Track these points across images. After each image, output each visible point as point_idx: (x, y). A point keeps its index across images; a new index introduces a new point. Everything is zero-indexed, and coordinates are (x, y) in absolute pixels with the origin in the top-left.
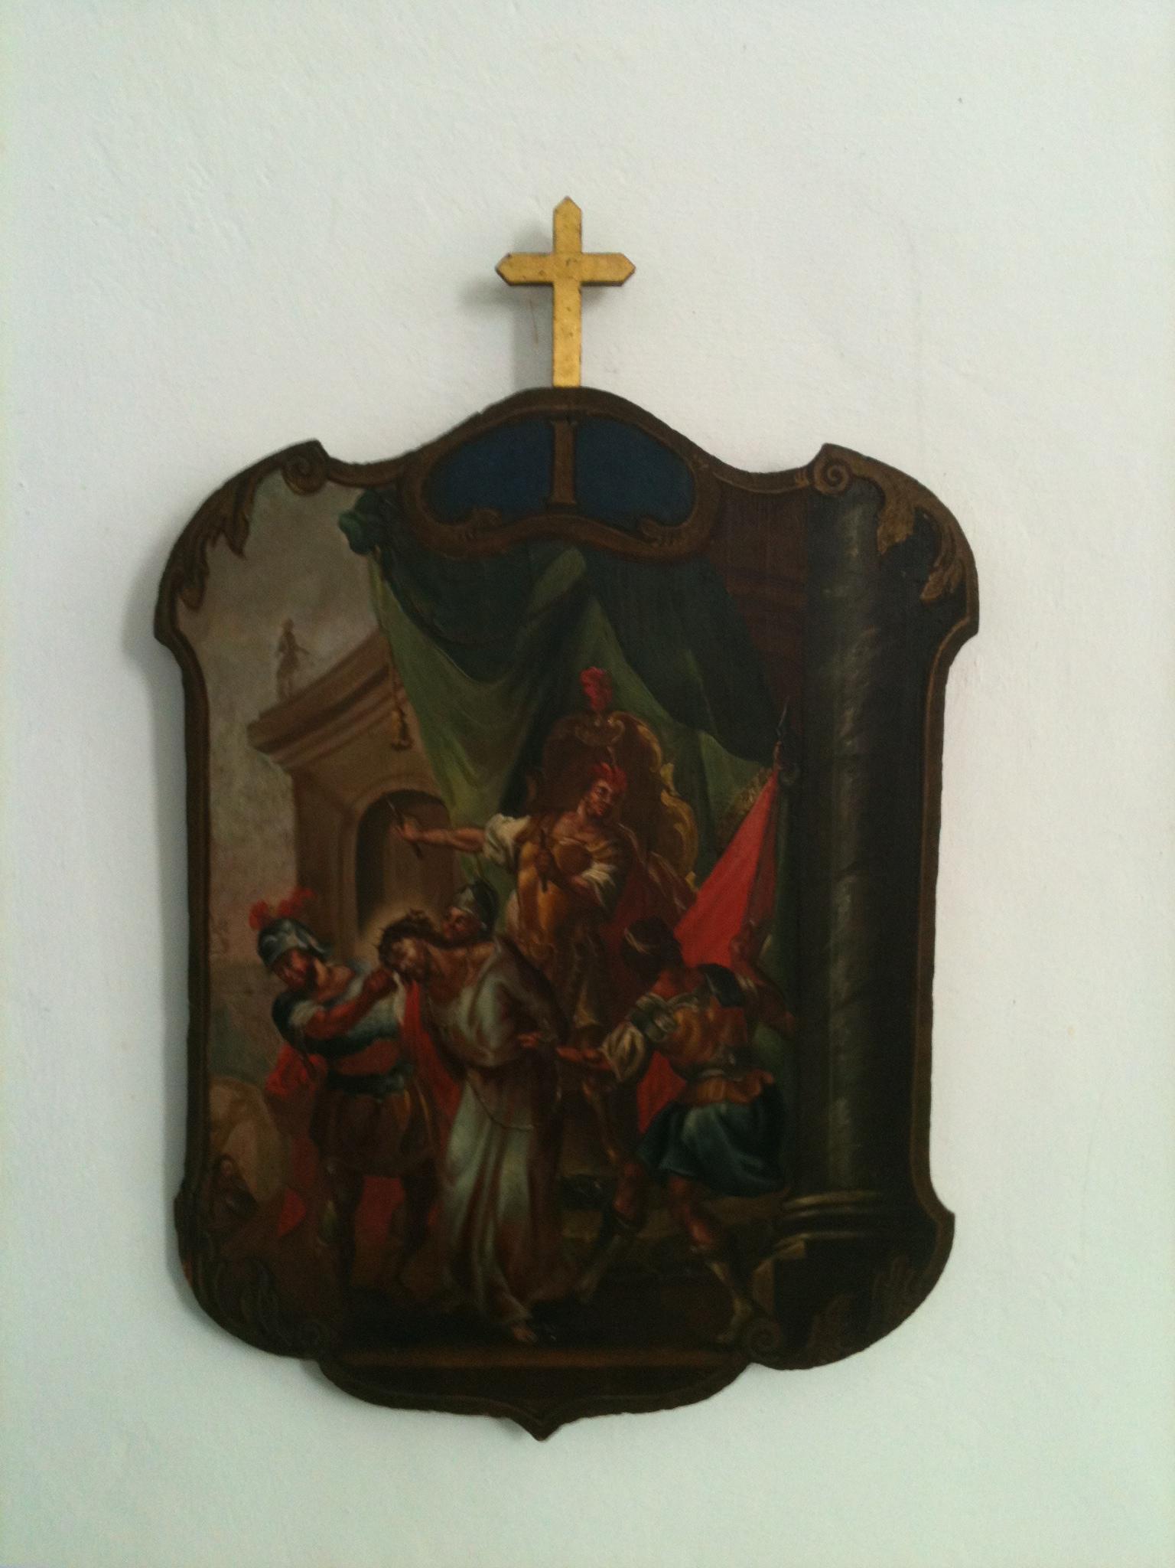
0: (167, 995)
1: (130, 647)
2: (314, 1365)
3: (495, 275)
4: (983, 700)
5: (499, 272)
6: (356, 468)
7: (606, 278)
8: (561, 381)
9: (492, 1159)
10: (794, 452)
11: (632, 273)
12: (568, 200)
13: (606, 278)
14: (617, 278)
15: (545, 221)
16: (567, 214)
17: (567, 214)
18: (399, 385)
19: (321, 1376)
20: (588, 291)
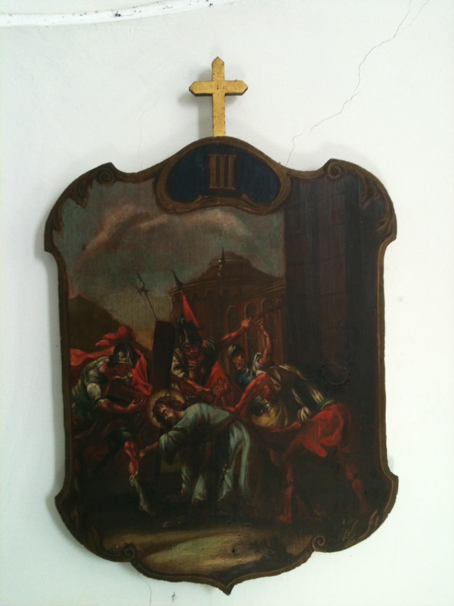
0: (55, 399)
1: (37, 254)
2: (129, 564)
3: (189, 91)
4: (398, 264)
5: (190, 90)
6: (133, 175)
7: (236, 91)
8: (218, 134)
9: (190, 577)
10: (316, 163)
11: (247, 89)
12: (217, 58)
13: (236, 91)
14: (238, 91)
15: (208, 65)
16: (218, 64)
17: (218, 64)
18: (147, 134)
19: (85, 549)
20: (227, 97)
